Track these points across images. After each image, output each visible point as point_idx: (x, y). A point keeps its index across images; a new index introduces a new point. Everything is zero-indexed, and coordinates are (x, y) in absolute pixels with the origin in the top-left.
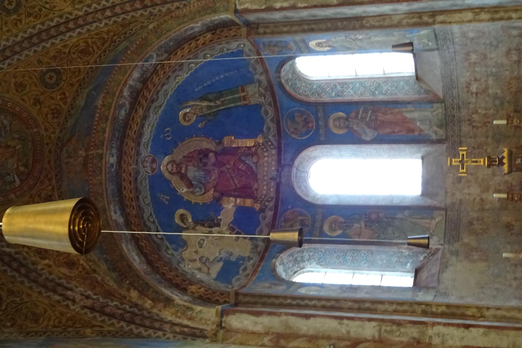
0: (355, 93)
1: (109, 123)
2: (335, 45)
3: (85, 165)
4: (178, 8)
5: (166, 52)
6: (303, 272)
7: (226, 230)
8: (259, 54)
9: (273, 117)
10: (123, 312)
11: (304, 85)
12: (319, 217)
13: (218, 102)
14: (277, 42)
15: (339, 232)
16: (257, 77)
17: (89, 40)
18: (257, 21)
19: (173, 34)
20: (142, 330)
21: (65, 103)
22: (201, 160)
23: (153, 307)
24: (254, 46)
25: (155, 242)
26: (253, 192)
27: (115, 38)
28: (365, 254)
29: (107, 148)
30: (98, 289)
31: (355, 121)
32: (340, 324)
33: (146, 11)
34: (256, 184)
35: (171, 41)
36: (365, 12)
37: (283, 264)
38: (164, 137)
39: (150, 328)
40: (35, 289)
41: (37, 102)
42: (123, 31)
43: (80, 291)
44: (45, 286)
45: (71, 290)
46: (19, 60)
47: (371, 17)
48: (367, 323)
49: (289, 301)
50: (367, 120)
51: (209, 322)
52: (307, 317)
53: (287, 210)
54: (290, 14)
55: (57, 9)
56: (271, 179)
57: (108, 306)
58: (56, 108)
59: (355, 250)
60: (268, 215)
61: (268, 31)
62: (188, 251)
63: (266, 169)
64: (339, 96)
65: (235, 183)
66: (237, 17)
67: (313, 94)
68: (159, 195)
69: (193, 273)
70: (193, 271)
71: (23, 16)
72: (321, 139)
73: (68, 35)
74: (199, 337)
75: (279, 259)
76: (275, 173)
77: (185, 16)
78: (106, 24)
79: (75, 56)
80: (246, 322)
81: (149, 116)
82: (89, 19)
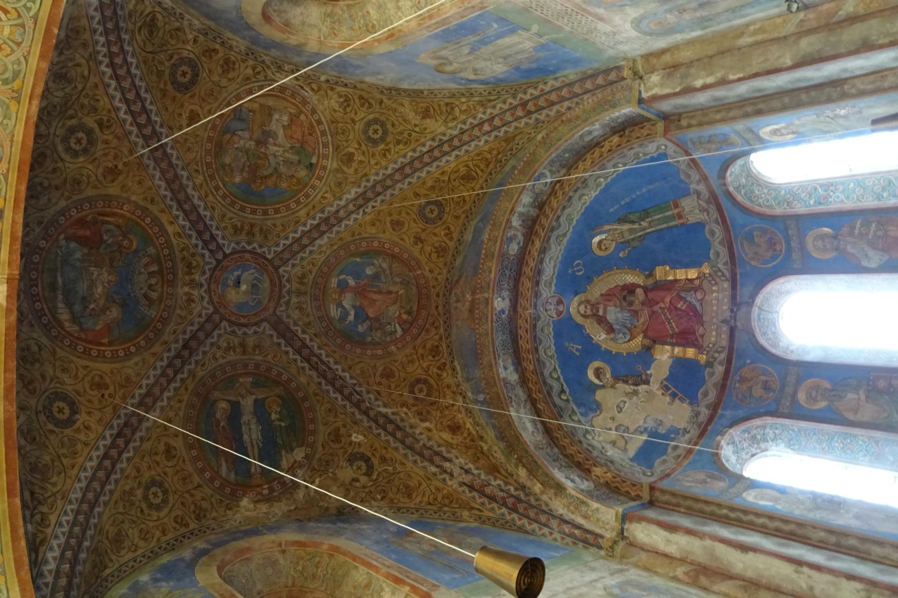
0: (848, 198)
1: (495, 261)
2: (801, 130)
3: (471, 311)
4: (569, 108)
5: (563, 167)
6: (766, 456)
7: (658, 389)
8: (688, 153)
9: (723, 239)
10: (506, 495)
11: (766, 191)
12: (791, 379)
13: (644, 224)
14: (710, 136)
15: (823, 404)
16: (693, 186)
17: (470, 164)
18: (677, 111)
19: (564, 145)
20: (525, 521)
21: (451, 239)
22: (624, 298)
23: (543, 493)
24: (678, 146)
25: (555, 405)
26: (697, 339)
27: (500, 157)
28: (864, 442)
29: (493, 291)
30: (482, 462)
31: (849, 239)
32: (796, 572)
33: (530, 118)
34: (702, 328)
35: (565, 151)
36: (845, 70)
37: (733, 443)
38: (574, 272)
39: (536, 521)
40: (411, 458)
41: (418, 240)
42: (508, 148)
43: (460, 463)
44: (421, 455)
45: (450, 461)
46: (392, 195)
47: (860, 76)
48: (844, 582)
49: (725, 511)
50: (870, 237)
51: (607, 527)
52: (744, 548)
53: (745, 364)
54: (720, 93)
55: (428, 131)
56: (723, 322)
57: (489, 485)
58: (440, 246)
59: (847, 434)
60: (716, 370)
61: (694, 122)
62: (601, 416)
63: (715, 308)
64: (820, 204)
65: (672, 327)
66: (644, 109)
67: (779, 203)
68: (567, 344)
69: (603, 448)
70: (604, 444)
71: (391, 146)
72: (795, 266)
73: (444, 159)
74: (592, 545)
75: (727, 436)
76: (728, 314)
77: (578, 117)
78: (486, 141)
79: (457, 184)
80: (654, 536)
81: (550, 248)
82: (466, 138)
